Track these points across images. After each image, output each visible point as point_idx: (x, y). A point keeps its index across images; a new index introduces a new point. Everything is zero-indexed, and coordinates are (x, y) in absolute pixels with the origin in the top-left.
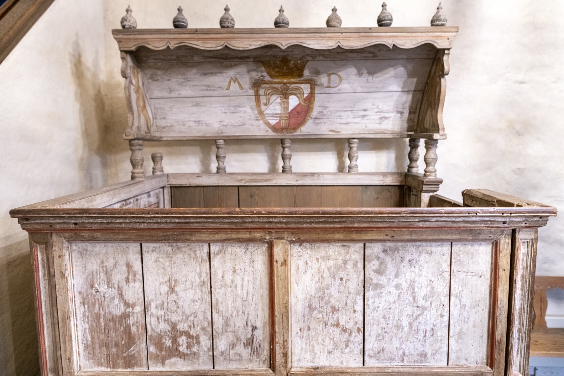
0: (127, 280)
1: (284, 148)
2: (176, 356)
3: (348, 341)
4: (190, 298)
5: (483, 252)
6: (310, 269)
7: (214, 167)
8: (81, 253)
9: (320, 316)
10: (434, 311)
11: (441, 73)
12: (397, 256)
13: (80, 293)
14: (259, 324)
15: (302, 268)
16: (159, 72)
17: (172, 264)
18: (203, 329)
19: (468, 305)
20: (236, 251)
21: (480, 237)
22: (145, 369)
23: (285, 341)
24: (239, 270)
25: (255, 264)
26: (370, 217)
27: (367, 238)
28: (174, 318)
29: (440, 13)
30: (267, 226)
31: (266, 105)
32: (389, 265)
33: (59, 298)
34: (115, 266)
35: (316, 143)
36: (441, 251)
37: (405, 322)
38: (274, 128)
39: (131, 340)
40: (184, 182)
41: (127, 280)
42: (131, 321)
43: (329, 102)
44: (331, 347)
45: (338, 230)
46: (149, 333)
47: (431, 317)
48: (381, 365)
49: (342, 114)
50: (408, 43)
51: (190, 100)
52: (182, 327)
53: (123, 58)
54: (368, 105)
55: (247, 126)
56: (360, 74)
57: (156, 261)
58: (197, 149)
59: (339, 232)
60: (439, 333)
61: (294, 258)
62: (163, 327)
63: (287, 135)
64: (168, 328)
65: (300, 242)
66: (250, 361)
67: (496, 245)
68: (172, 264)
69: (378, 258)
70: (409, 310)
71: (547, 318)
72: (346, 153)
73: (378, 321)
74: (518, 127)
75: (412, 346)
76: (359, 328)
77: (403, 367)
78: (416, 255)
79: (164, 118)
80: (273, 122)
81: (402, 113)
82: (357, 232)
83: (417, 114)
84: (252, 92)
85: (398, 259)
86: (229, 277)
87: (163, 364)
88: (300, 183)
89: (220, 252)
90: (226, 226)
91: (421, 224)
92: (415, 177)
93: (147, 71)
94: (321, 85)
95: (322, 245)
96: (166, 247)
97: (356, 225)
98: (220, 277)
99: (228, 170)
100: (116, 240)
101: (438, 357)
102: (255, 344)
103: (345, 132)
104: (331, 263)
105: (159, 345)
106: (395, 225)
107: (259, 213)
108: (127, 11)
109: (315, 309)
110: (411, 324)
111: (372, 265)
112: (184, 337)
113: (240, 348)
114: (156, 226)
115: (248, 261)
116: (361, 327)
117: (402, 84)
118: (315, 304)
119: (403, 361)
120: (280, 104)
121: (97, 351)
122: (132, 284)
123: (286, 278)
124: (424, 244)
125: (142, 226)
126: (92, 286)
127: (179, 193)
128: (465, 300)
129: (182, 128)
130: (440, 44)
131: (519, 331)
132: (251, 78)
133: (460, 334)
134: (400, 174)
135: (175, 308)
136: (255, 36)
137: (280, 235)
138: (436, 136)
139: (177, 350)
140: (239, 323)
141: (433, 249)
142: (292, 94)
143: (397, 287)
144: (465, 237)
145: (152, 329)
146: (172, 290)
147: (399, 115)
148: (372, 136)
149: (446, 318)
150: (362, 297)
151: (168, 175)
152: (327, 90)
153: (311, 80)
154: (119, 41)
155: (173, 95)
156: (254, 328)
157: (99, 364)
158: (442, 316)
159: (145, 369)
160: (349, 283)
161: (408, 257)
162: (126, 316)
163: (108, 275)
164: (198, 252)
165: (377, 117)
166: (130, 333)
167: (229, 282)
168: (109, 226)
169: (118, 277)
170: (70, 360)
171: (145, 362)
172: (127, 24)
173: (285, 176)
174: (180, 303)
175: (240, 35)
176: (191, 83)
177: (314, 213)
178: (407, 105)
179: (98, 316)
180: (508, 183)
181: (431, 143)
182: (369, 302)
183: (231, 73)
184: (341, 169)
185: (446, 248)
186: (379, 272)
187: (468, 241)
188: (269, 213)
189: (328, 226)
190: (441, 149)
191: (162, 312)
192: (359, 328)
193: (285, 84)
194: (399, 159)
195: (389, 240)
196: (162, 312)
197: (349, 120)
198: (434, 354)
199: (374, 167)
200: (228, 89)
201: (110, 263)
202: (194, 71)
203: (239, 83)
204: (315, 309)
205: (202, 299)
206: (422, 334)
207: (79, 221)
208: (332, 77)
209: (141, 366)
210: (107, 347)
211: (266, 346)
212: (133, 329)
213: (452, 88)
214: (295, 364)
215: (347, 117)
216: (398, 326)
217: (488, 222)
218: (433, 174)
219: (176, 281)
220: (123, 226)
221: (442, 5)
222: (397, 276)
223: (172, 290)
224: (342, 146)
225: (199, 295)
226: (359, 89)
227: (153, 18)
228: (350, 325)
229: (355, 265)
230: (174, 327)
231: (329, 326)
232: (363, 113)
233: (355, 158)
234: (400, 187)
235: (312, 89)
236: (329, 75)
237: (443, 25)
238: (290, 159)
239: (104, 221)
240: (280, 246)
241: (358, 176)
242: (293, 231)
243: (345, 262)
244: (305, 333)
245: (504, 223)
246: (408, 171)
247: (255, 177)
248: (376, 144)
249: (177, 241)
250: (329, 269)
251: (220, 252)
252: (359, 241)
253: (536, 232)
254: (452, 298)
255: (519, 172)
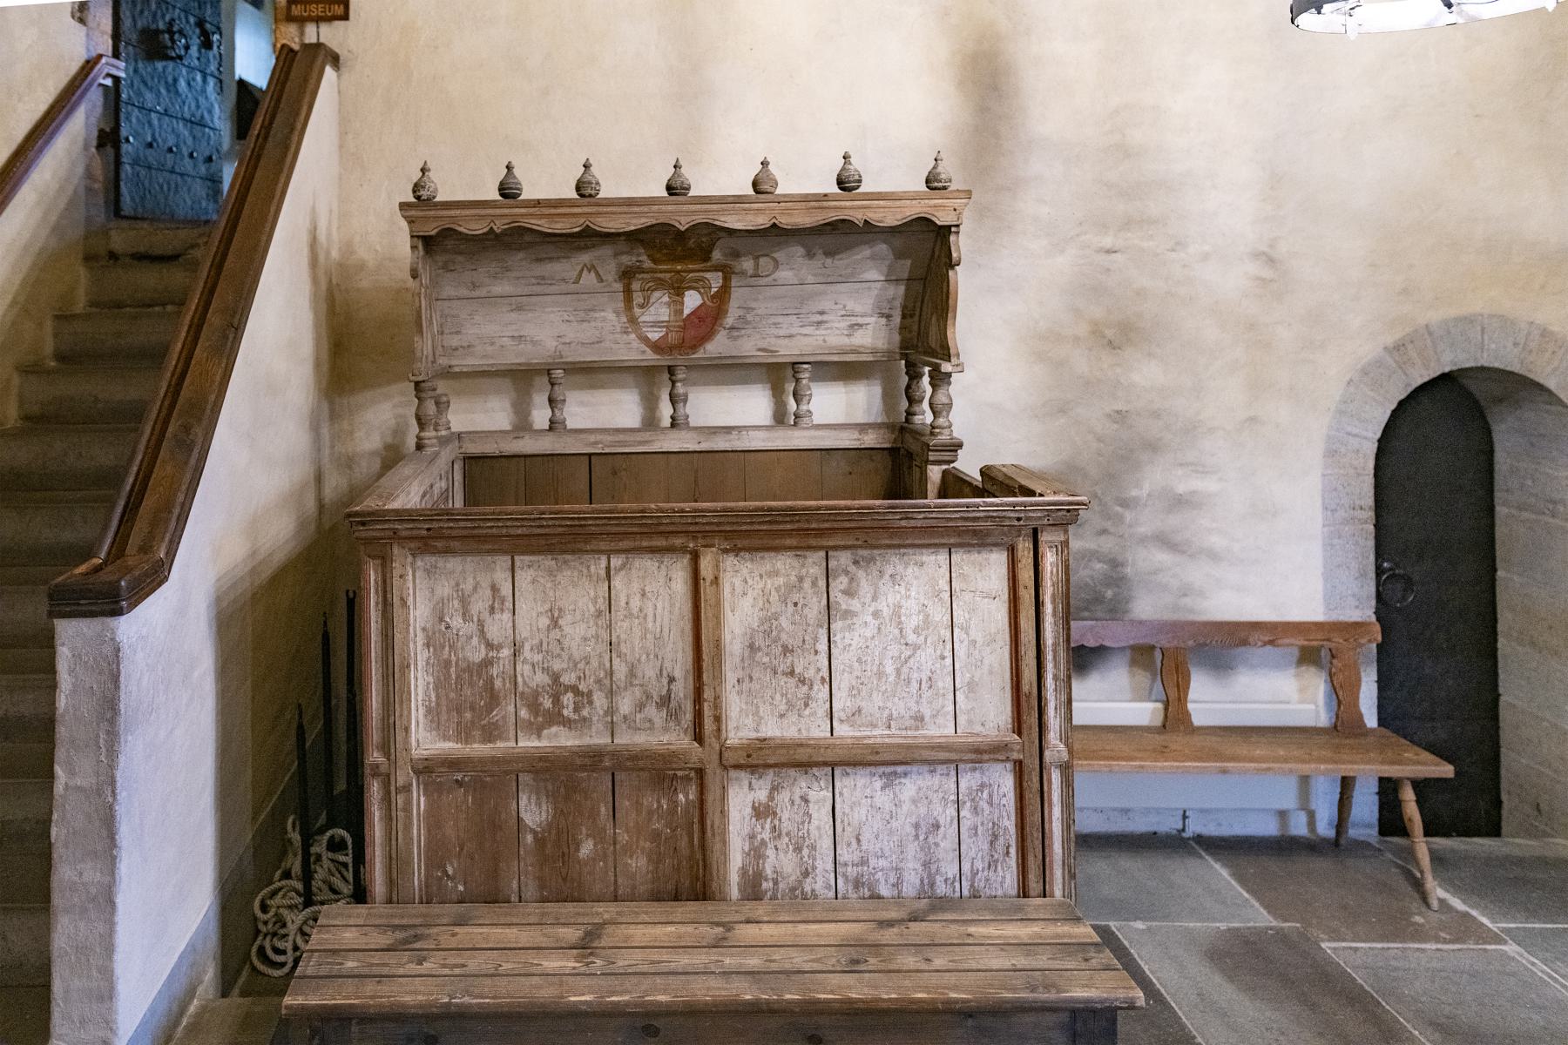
0: (492, 610)
1: (674, 383)
2: (558, 724)
3: (808, 697)
4: (578, 633)
5: (996, 562)
6: (749, 591)
7: (541, 416)
8: (428, 572)
9: (766, 659)
10: (930, 650)
11: (944, 260)
12: (874, 569)
13: (424, 629)
14: (678, 674)
15: (739, 590)
16: (460, 258)
17: (556, 585)
18: (598, 681)
19: (980, 641)
20: (646, 565)
21: (989, 540)
22: (512, 744)
23: (717, 698)
24: (652, 592)
25: (673, 584)
26: (835, 515)
27: (831, 543)
28: (557, 666)
29: (940, 169)
30: (691, 528)
31: (642, 306)
32: (863, 583)
33: (398, 636)
34: (475, 589)
35: (733, 371)
36: (935, 562)
37: (890, 668)
38: (656, 347)
39: (493, 699)
40: (490, 448)
41: (492, 610)
42: (495, 671)
43: (756, 300)
44: (783, 707)
45: (789, 533)
46: (520, 688)
47: (926, 659)
48: (858, 734)
49: (780, 319)
50: (890, 217)
51: (507, 301)
52: (568, 679)
53: (414, 247)
54: (826, 304)
55: (607, 344)
56: (810, 255)
57: (533, 581)
58: (506, 383)
59: (790, 536)
60: (940, 684)
61: (728, 575)
62: (541, 679)
63: (678, 359)
64: (547, 680)
65: (736, 551)
66: (666, 730)
67: (1012, 551)
68: (556, 585)
69: (847, 573)
70: (894, 650)
71: (1190, 706)
72: (790, 387)
73: (851, 667)
74: (1109, 333)
75: (901, 704)
76: (823, 679)
77: (889, 736)
78: (900, 568)
79: (458, 333)
80: (655, 335)
81: (888, 317)
82: (816, 536)
83: (916, 318)
84: (619, 286)
85: (876, 573)
86: (636, 603)
87: (539, 737)
88: (704, 446)
89: (623, 566)
90: (635, 529)
91: (903, 523)
92: (917, 434)
93: (438, 258)
94: (743, 273)
95: (766, 555)
96: (548, 562)
97: (814, 526)
98: (623, 604)
99: (570, 424)
100: (479, 552)
101: (940, 720)
102: (673, 704)
103: (787, 350)
104: (781, 581)
105: (534, 707)
106: (868, 524)
107: (683, 511)
108: (423, 170)
109: (759, 649)
110: (898, 671)
111: (839, 583)
112: (570, 695)
113: (651, 711)
114: (539, 531)
115: (662, 580)
116: (826, 675)
117: (885, 269)
118: (759, 642)
119: (889, 727)
120: (668, 304)
121: (444, 717)
122: (497, 616)
123: (718, 604)
124: (910, 551)
125: (519, 532)
126: (441, 620)
127: (483, 471)
128: (976, 634)
129: (490, 348)
130: (942, 219)
131: (1056, 678)
132: (619, 265)
133: (972, 686)
134: (890, 427)
135: (558, 651)
136: (636, 209)
137: (709, 541)
138: (946, 367)
139: (560, 714)
140: (649, 671)
141: (924, 558)
142: (690, 288)
143: (876, 614)
144: (967, 539)
145: (525, 683)
146: (555, 623)
147: (884, 321)
148: (836, 358)
149: (949, 661)
150: (825, 631)
151: (459, 436)
152: (753, 281)
153: (725, 266)
154: (411, 221)
155: (477, 293)
156: (672, 680)
157: (446, 738)
158: (943, 658)
159: (512, 744)
160: (806, 610)
161: (889, 570)
162: (487, 663)
163: (465, 602)
164: (593, 568)
165: (844, 324)
166: (492, 688)
167: (635, 611)
168: (476, 532)
169: (479, 605)
170: (407, 730)
171: (512, 733)
172: (424, 194)
173: (675, 434)
174: (566, 643)
175: (609, 209)
176: (514, 274)
177: (756, 509)
178: (898, 303)
179: (447, 663)
180: (1099, 440)
181: (939, 379)
182: (836, 638)
183: (585, 257)
184: (780, 418)
185: (942, 557)
186: (849, 593)
187: (973, 546)
188: (696, 511)
189: (775, 527)
190: (959, 387)
191: (540, 657)
192: (823, 679)
193: (678, 272)
194: (888, 397)
195: (861, 547)
196: (540, 657)
197: (794, 331)
198: (934, 716)
199: (840, 411)
200: (577, 282)
201: (468, 586)
202: (521, 255)
203: (597, 273)
204: (759, 649)
205: (597, 637)
206: (915, 685)
207: (435, 525)
208: (762, 261)
209: (508, 739)
210: (459, 710)
211: (688, 706)
212: (498, 683)
213: (968, 283)
214: (731, 734)
215: (790, 325)
216: (880, 674)
217: (997, 519)
218: (946, 432)
219: (560, 610)
220: (494, 531)
221: (942, 155)
222: (875, 598)
223: (555, 623)
224: (782, 377)
225: (593, 631)
226: (810, 279)
227: (466, 182)
228: (810, 674)
229: (814, 584)
230: (556, 678)
231: (779, 676)
232: (819, 318)
233: (805, 400)
234: (893, 451)
235: (726, 279)
236: (757, 258)
237: (945, 188)
238: (685, 401)
239: (469, 524)
240: (709, 558)
241: (812, 433)
242: (727, 535)
243: (801, 579)
244: (746, 685)
245: (1019, 519)
246: (907, 421)
247: (621, 437)
248: (844, 370)
249: (565, 552)
250: (778, 589)
251: (623, 566)
252: (820, 548)
253: (1066, 532)
254: (956, 630)
255: (1120, 417)
